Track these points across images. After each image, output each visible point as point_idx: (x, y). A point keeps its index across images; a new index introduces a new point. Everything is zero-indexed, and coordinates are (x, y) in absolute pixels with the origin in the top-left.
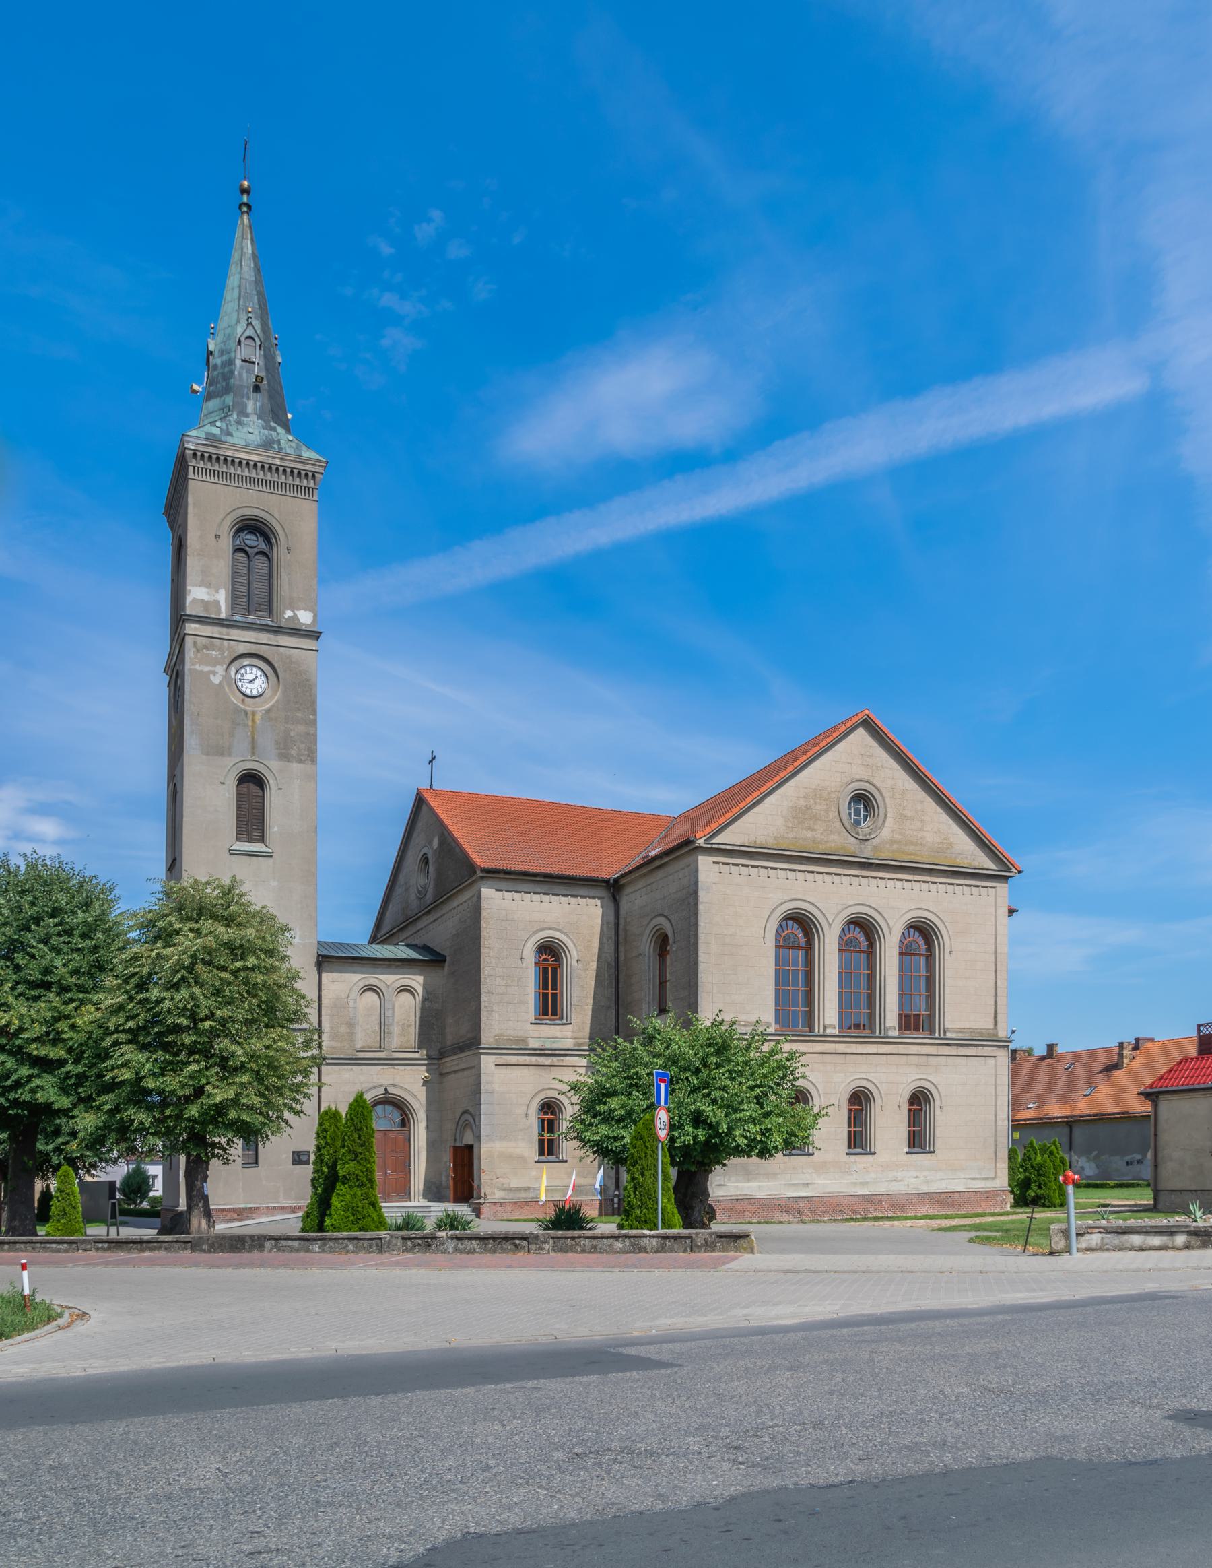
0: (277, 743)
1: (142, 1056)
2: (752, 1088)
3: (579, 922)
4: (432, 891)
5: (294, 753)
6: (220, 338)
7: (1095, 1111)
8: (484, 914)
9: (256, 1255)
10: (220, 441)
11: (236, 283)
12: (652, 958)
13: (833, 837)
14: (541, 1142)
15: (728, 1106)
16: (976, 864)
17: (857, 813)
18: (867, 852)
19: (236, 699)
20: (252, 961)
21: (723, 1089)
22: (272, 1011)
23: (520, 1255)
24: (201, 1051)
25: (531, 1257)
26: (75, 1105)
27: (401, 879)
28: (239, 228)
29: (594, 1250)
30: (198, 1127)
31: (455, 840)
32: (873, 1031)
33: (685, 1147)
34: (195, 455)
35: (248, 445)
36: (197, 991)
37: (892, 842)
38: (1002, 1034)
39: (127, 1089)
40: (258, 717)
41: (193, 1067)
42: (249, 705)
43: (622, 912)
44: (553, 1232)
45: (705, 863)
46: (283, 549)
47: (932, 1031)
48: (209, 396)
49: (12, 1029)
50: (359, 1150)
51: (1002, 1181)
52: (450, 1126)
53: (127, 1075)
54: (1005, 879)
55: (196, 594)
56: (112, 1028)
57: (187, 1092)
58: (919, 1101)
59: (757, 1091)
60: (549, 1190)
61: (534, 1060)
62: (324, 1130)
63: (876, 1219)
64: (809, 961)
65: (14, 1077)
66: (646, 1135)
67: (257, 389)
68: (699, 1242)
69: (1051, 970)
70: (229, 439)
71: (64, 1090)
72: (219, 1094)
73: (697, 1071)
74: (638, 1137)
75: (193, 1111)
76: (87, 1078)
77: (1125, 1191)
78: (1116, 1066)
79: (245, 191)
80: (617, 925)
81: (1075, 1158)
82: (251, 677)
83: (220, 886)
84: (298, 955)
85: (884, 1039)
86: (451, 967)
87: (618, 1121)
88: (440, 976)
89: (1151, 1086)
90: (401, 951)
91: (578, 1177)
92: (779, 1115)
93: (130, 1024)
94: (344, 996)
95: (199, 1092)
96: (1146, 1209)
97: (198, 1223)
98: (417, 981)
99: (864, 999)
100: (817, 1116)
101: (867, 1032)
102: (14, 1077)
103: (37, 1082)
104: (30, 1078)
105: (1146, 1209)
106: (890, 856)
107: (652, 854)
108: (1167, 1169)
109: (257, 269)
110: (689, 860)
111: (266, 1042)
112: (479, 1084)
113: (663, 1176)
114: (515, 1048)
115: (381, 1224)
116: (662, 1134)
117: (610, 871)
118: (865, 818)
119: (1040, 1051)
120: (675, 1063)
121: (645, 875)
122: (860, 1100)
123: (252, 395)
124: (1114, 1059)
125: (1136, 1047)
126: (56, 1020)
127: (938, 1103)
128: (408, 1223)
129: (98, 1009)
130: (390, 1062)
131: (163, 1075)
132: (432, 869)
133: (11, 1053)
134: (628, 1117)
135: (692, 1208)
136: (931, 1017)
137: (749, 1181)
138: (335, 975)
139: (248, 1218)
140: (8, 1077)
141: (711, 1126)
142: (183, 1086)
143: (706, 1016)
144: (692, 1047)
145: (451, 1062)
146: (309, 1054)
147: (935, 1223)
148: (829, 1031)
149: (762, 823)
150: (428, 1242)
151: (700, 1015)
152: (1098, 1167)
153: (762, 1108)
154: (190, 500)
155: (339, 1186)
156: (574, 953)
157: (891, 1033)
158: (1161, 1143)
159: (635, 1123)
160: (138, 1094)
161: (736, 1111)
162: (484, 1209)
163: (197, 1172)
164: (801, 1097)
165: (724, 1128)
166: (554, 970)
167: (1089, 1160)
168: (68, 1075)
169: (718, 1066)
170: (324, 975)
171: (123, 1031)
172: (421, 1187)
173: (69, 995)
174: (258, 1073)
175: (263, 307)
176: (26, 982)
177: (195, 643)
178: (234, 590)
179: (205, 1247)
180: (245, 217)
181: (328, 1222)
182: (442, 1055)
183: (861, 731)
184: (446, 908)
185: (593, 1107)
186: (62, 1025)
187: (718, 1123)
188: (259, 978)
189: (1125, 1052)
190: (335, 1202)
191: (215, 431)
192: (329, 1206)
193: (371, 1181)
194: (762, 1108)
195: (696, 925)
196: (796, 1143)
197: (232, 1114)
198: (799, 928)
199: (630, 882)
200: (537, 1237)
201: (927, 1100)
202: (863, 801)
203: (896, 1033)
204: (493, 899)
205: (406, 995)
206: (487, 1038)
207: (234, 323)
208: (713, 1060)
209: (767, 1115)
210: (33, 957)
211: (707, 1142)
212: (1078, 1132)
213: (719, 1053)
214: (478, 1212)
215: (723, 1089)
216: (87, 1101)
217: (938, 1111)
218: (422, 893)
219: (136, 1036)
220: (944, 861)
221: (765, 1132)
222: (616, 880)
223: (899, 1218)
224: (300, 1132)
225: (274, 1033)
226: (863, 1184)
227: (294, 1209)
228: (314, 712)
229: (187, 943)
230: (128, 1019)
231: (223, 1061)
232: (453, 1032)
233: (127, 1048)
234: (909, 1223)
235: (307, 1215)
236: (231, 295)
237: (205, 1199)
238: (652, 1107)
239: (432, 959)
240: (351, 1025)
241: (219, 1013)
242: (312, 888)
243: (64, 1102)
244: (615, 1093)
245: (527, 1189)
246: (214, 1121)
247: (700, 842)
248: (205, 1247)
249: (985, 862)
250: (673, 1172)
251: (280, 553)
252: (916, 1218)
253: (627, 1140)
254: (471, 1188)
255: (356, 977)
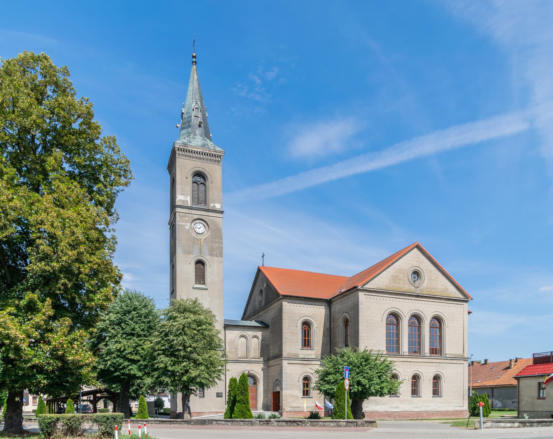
0: (209, 250)
1: (167, 359)
2: (377, 373)
3: (317, 314)
4: (264, 302)
5: (215, 253)
6: (186, 108)
7: (501, 384)
8: (283, 311)
9: (210, 426)
10: (187, 145)
11: (192, 89)
12: (342, 328)
13: (406, 286)
14: (304, 391)
15: (369, 379)
16: (457, 296)
17: (414, 278)
18: (418, 292)
19: (194, 235)
20: (204, 327)
21: (367, 373)
22: (211, 344)
23: (299, 427)
24: (187, 358)
25: (303, 428)
26: (143, 375)
27: (253, 297)
28: (192, 70)
29: (324, 426)
30: (186, 384)
31: (272, 285)
32: (420, 354)
33: (354, 392)
34: (178, 149)
35: (197, 146)
36: (185, 338)
37: (427, 288)
38: (466, 356)
39: (161, 371)
40: (202, 241)
41: (184, 364)
42: (199, 237)
43: (332, 311)
44: (310, 420)
45: (361, 294)
46: (210, 182)
47: (441, 354)
48: (183, 128)
49: (122, 349)
50: (244, 392)
51: (466, 407)
52: (271, 385)
53: (162, 365)
54: (467, 301)
55: (180, 198)
56: (157, 349)
57: (183, 371)
58: (437, 378)
59: (379, 374)
60: (307, 407)
61: (301, 362)
62: (231, 385)
63: (421, 420)
64: (398, 329)
65: (123, 365)
66: (341, 388)
67: (200, 126)
68: (359, 424)
69: (492, 332)
70: (190, 144)
71: (140, 370)
72: (194, 373)
73: (359, 367)
74: (339, 389)
75: (185, 378)
76: (148, 366)
77: (511, 412)
78: (509, 368)
79: (194, 57)
80: (330, 315)
81: (494, 400)
82: (199, 227)
83: (192, 301)
84: (218, 326)
85: (424, 357)
86: (272, 329)
87: (332, 383)
88: (268, 332)
89: (517, 375)
90: (253, 323)
91: (317, 401)
92: (387, 382)
93: (163, 348)
94: (234, 338)
95: (187, 371)
96: (516, 417)
97: (187, 416)
98: (259, 334)
99: (417, 343)
100: (400, 383)
101: (418, 354)
102: (123, 365)
103: (130, 367)
104: (128, 365)
105: (516, 417)
106: (426, 293)
107: (343, 291)
108: (522, 404)
109: (199, 84)
110: (356, 293)
111: (209, 355)
112: (282, 370)
113: (347, 402)
114: (294, 358)
115: (251, 417)
116: (347, 388)
117: (328, 297)
118: (417, 279)
119: (483, 362)
120: (351, 364)
121: (340, 298)
122: (416, 378)
123: (198, 128)
124: (508, 365)
125: (516, 361)
126: (137, 346)
127: (443, 380)
128: (259, 417)
129: (151, 343)
130: (250, 362)
131: (174, 365)
132: (264, 294)
133: (121, 357)
134: (335, 382)
135: (357, 413)
136: (441, 350)
137: (377, 405)
138: (231, 331)
139: (201, 415)
140: (120, 365)
141: (363, 386)
142: (181, 370)
143: (361, 348)
144: (357, 359)
145: (272, 362)
146: (223, 359)
147: (441, 421)
148: (405, 354)
149: (381, 281)
150: (268, 422)
151: (360, 348)
152: (502, 404)
153: (381, 380)
154: (177, 165)
155: (237, 404)
156: (315, 325)
157: (427, 355)
158: (520, 395)
159: (338, 384)
160: (165, 371)
161: (372, 381)
162: (284, 414)
163: (186, 399)
164: (395, 376)
165: (368, 386)
166: (308, 331)
167: (499, 401)
168: (141, 365)
169: (366, 365)
170: (227, 331)
171: (160, 350)
172: (261, 406)
173: (141, 338)
174: (207, 366)
175: (201, 97)
176: (126, 333)
177: (180, 215)
178: (193, 196)
179: (192, 423)
180: (194, 66)
181: (233, 415)
182: (269, 359)
183: (416, 249)
184: (269, 308)
185: (323, 378)
186: (139, 348)
187: (366, 385)
188: (206, 333)
189: (512, 363)
190: (235, 409)
191: (186, 141)
192: (233, 410)
193: (248, 402)
194: (381, 380)
195: (358, 316)
196: (393, 392)
197: (198, 380)
198: (395, 316)
199: (335, 301)
200: (305, 421)
201: (439, 378)
202: (417, 273)
203: (429, 355)
204: (287, 306)
205: (255, 338)
206: (285, 354)
207: (191, 103)
208: (364, 363)
209: (382, 382)
210: (128, 324)
211: (362, 391)
212: (495, 391)
213: (366, 361)
214: (281, 415)
215: (367, 373)
216: (148, 374)
217: (422, 382)
218: (260, 303)
219: (165, 352)
220: (445, 295)
221: (382, 388)
222: (330, 300)
223: (429, 420)
224: (221, 386)
225: (212, 352)
226: (417, 407)
227: (222, 412)
228: (222, 239)
229: (181, 320)
230: (162, 346)
231: (195, 361)
232: (273, 351)
233: (162, 356)
234: (432, 421)
235: (226, 413)
236: (190, 93)
237: (189, 408)
238: (343, 379)
239: (265, 326)
240: (236, 349)
241: (193, 345)
242: (221, 300)
243: (140, 374)
244: (331, 374)
245: (299, 407)
246: (192, 381)
247: (359, 287)
248: (192, 423)
249: (460, 296)
250: (350, 401)
251: (208, 183)
252: (435, 419)
253: (335, 390)
254: (279, 406)
255: (238, 332)
